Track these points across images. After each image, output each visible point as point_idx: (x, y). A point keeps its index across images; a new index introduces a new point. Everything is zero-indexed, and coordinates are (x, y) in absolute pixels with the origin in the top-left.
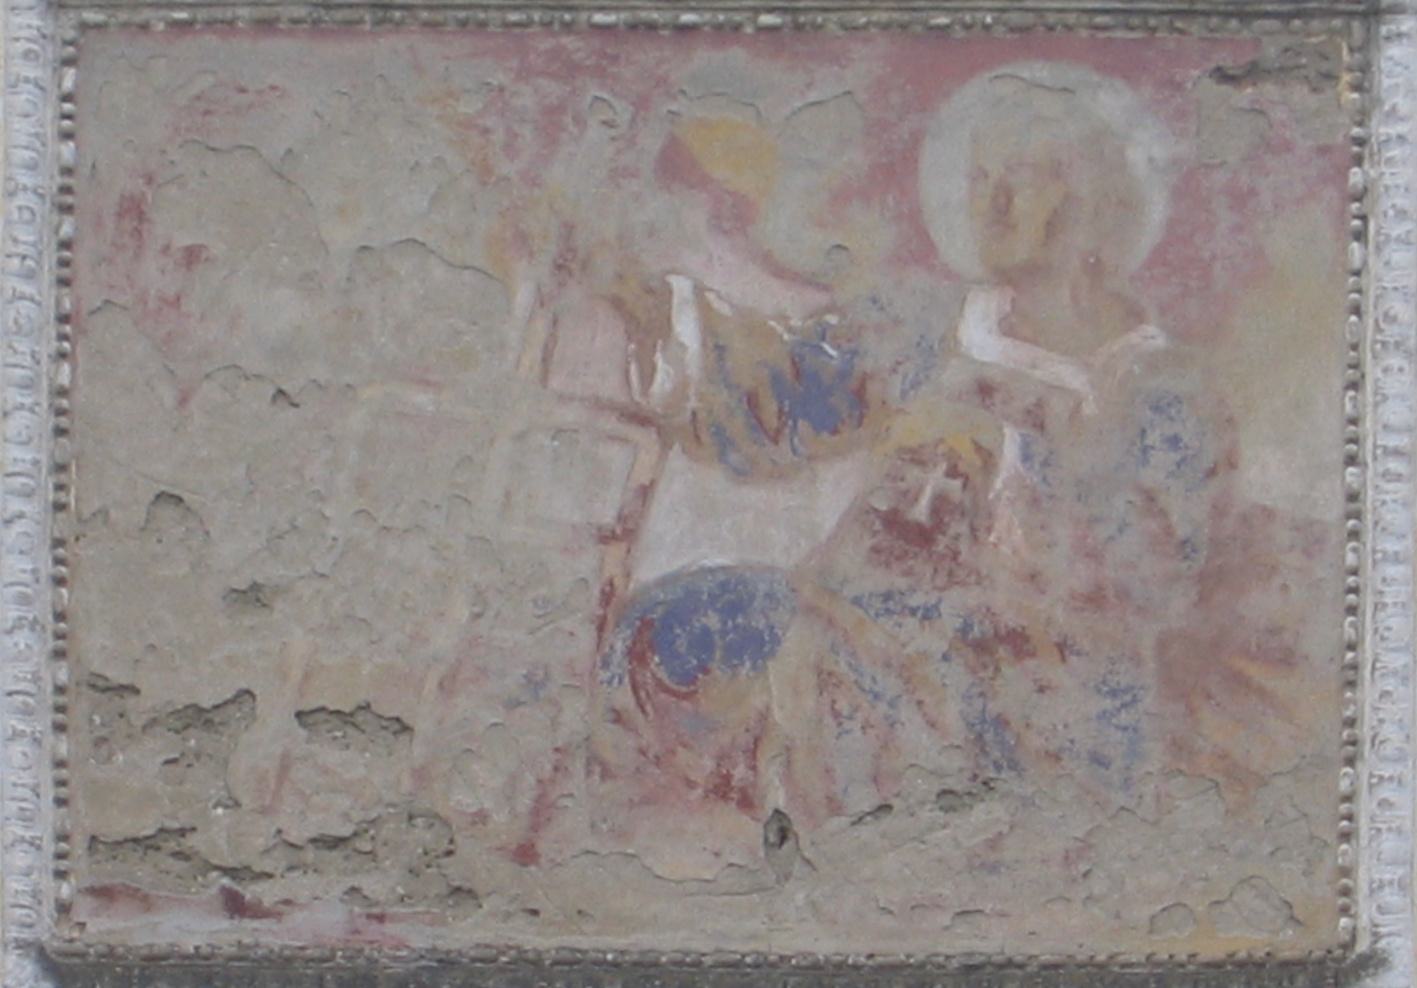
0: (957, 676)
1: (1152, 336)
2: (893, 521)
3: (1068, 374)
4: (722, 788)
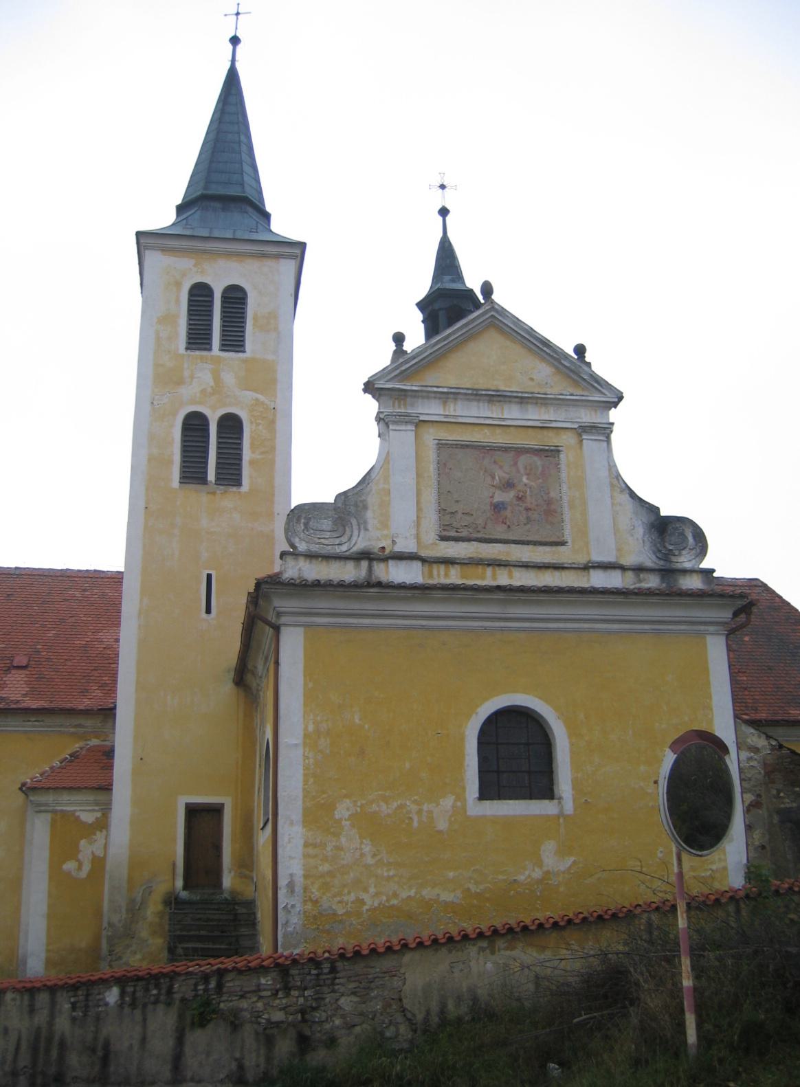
1: (540, 481)
2: (517, 497)
3: (533, 484)
4: (503, 522)
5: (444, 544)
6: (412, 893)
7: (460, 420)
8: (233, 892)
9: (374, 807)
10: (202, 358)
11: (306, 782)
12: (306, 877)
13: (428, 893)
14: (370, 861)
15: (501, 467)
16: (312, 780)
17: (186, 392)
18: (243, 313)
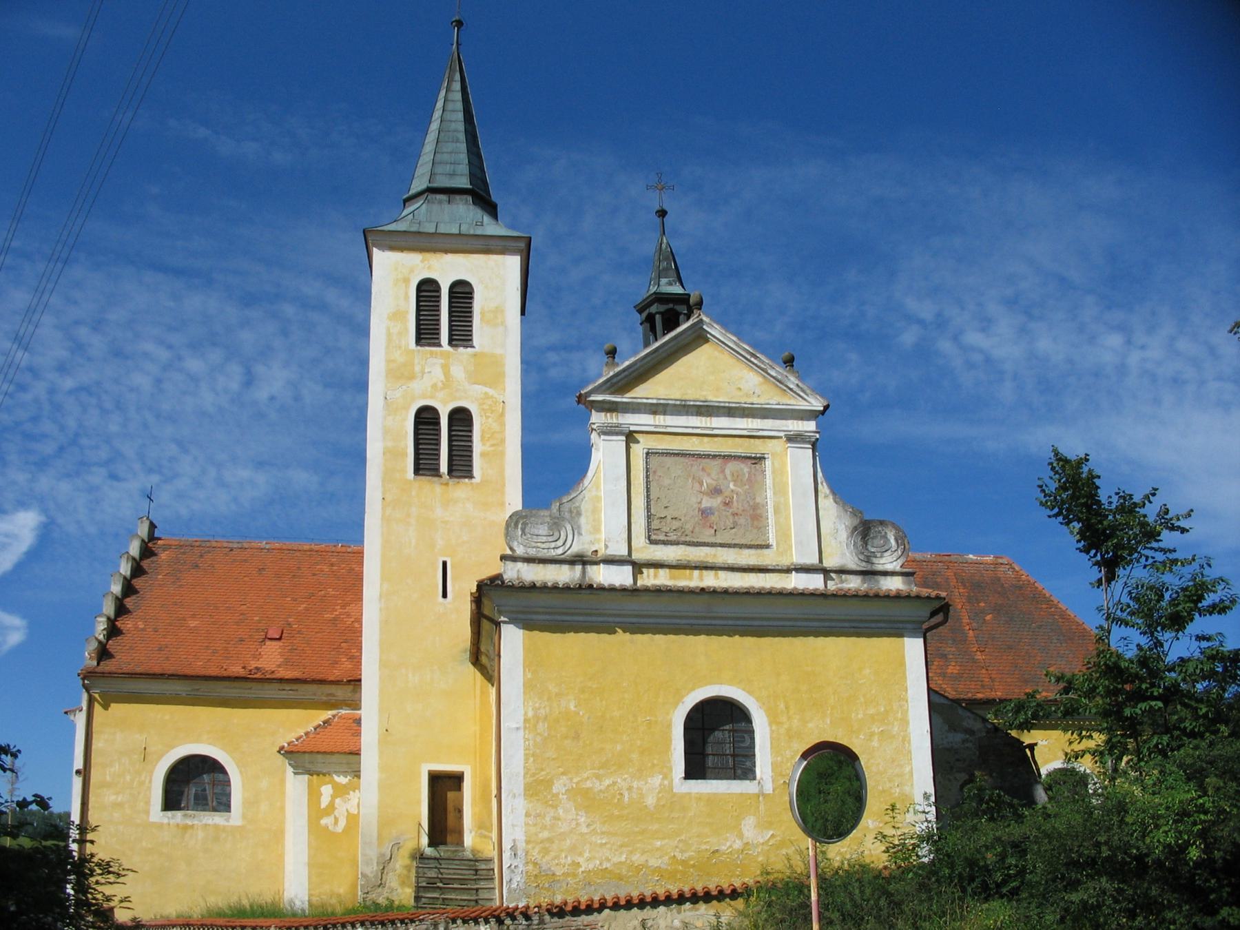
0: (731, 517)
1: (747, 487)
3: (740, 490)
4: (710, 527)
5: (653, 547)
6: (623, 859)
7: (669, 430)
8: (473, 851)
9: (588, 784)
10: (431, 353)
11: (526, 760)
12: (528, 842)
13: (637, 859)
14: (584, 830)
15: (709, 475)
16: (532, 759)
17: (418, 386)
18: (471, 308)
